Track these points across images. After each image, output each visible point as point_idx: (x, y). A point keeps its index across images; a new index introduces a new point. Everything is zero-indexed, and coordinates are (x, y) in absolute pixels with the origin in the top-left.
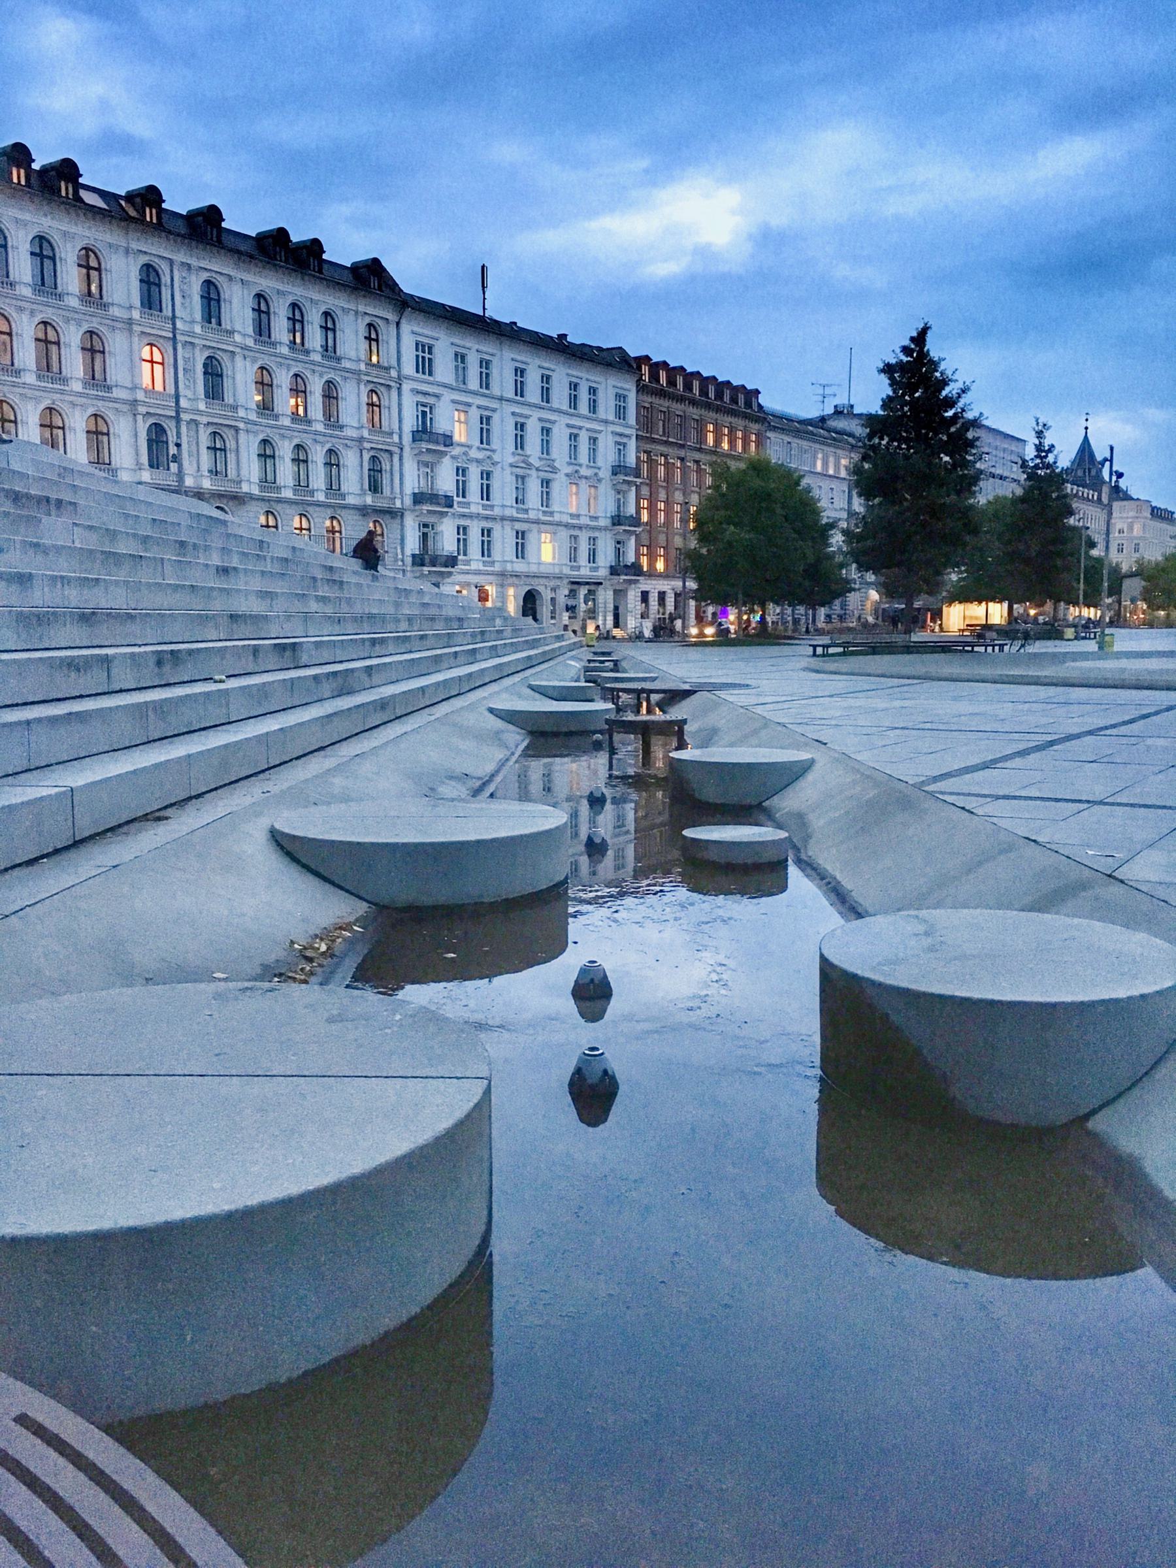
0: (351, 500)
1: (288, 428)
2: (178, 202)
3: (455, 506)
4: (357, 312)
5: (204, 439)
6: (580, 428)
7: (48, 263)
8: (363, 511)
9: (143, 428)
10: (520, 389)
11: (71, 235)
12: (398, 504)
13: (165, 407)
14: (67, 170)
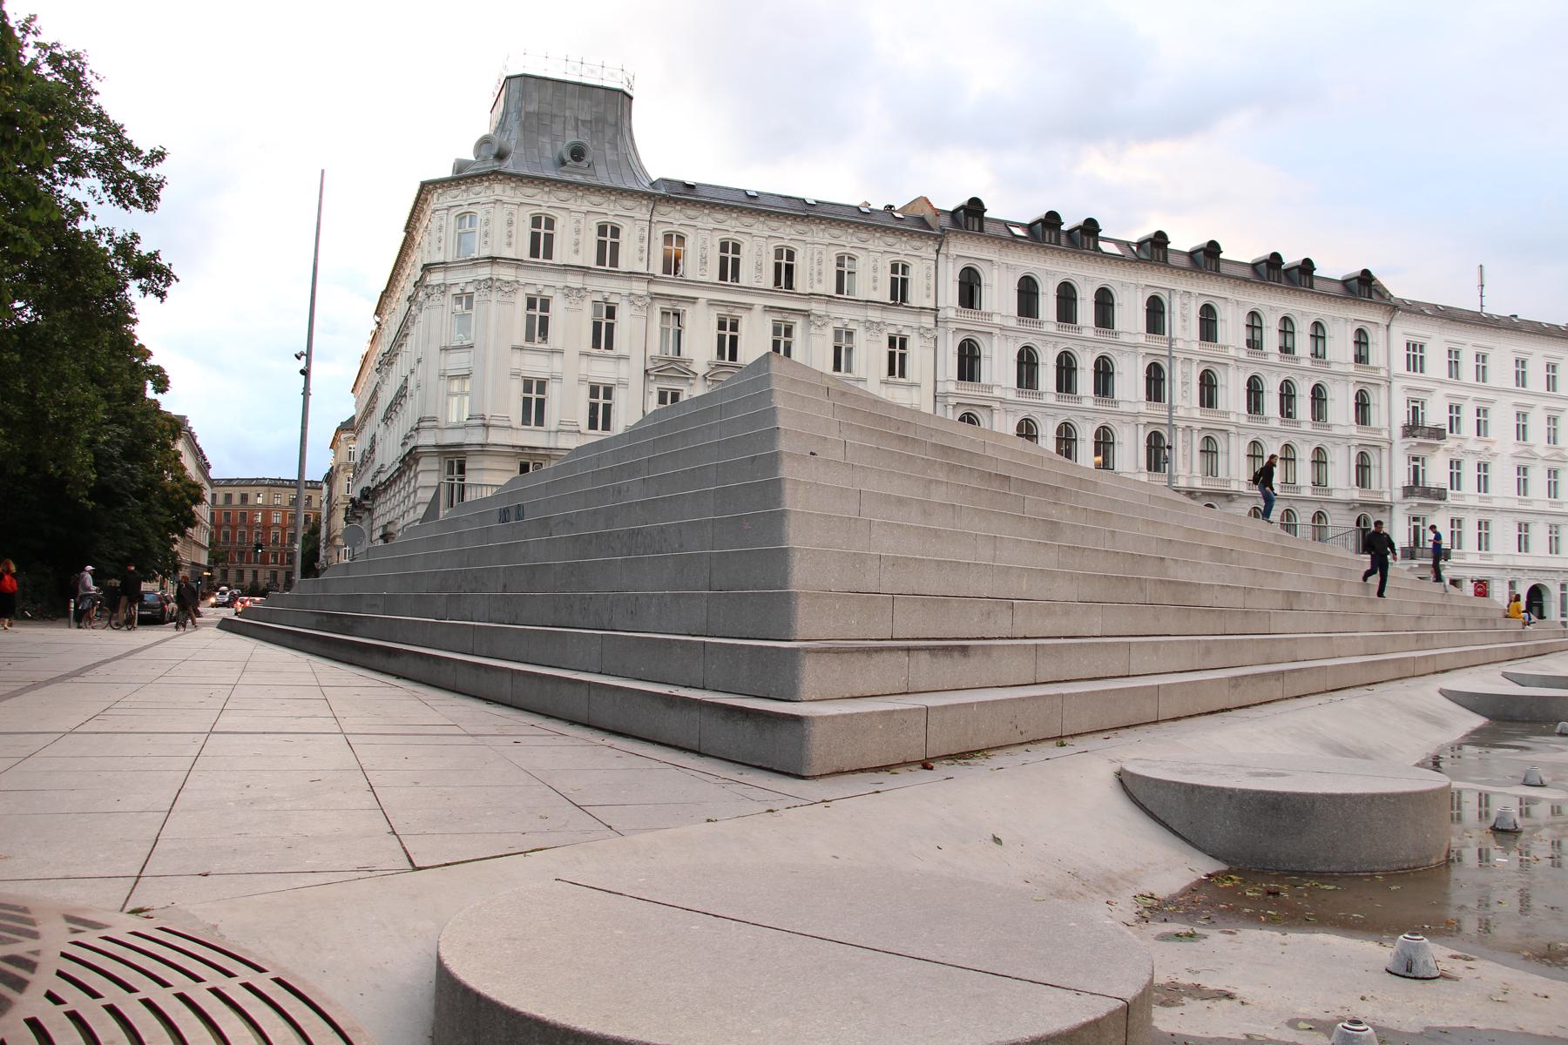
0: (1336, 495)
1: (1276, 430)
2: (1183, 240)
3: (1449, 498)
4: (1137, 286)
5: (1197, 444)
6: (1466, 398)
7: (1320, 342)
8: (1350, 505)
9: (1354, 453)
10: (1521, 378)
11: (1304, 311)
12: (1387, 498)
13: (1162, 417)
14: (1307, 266)
